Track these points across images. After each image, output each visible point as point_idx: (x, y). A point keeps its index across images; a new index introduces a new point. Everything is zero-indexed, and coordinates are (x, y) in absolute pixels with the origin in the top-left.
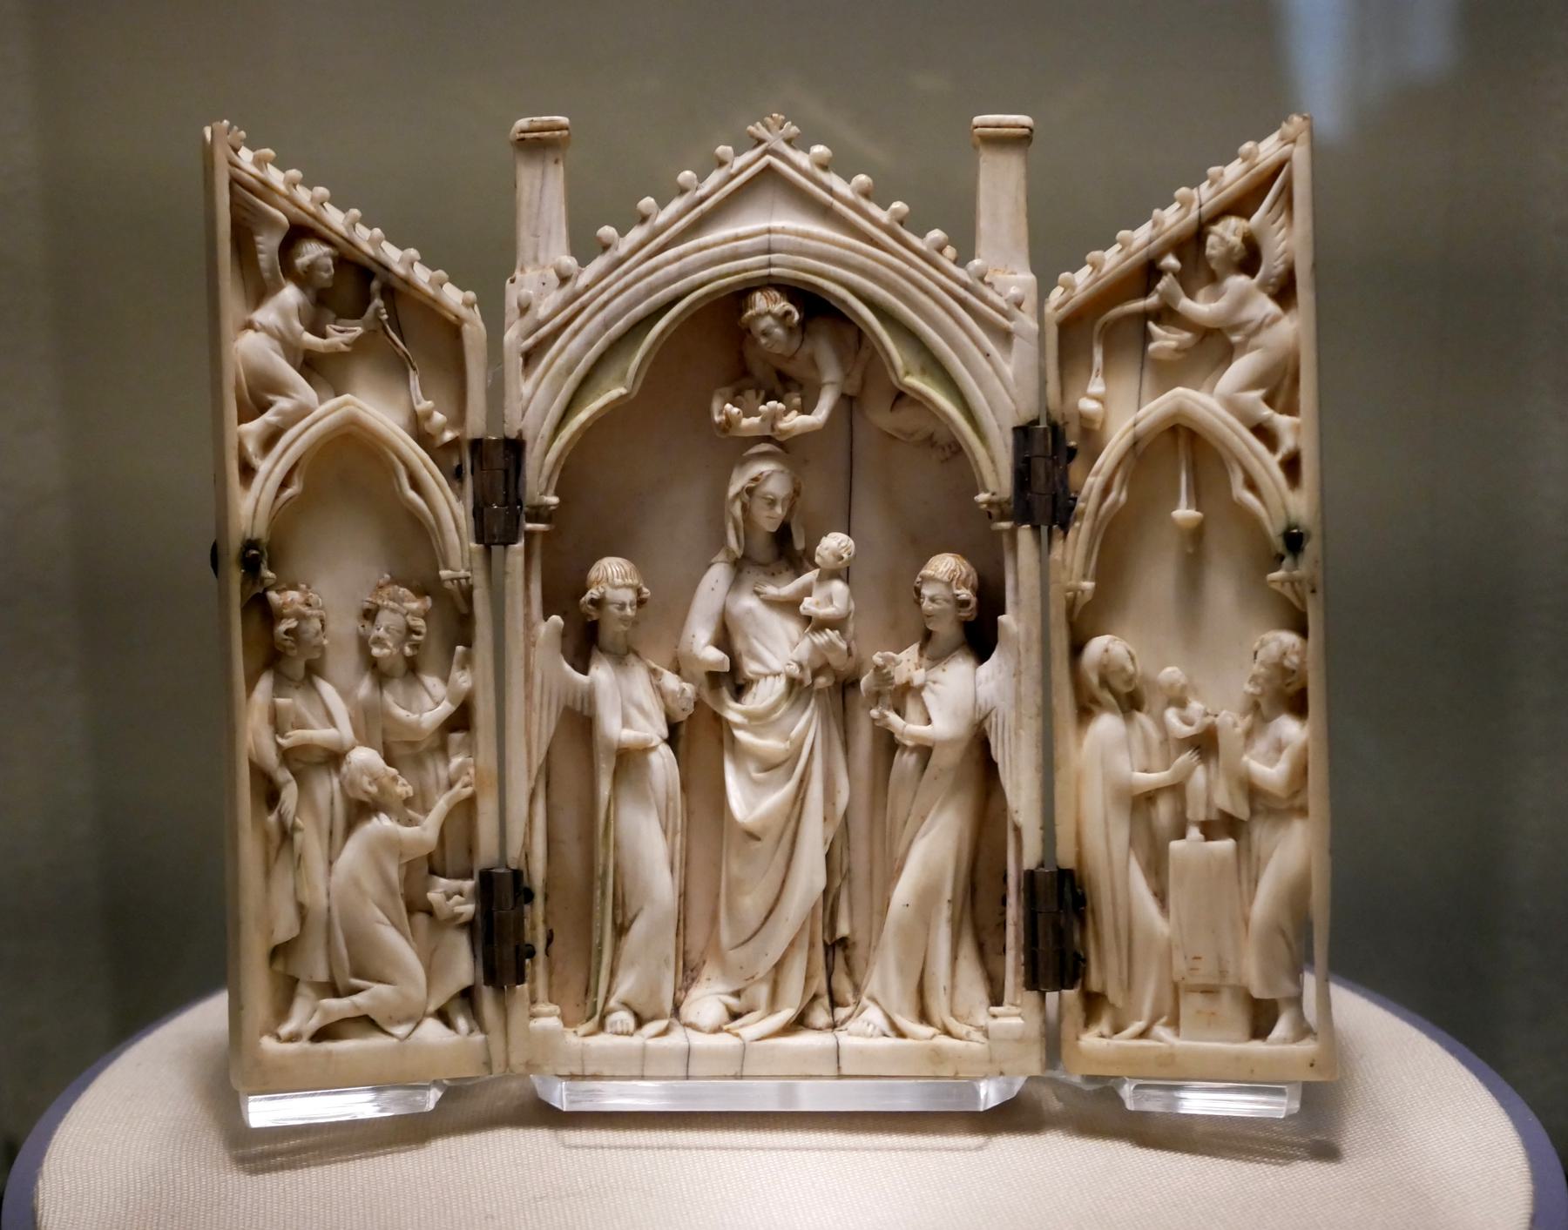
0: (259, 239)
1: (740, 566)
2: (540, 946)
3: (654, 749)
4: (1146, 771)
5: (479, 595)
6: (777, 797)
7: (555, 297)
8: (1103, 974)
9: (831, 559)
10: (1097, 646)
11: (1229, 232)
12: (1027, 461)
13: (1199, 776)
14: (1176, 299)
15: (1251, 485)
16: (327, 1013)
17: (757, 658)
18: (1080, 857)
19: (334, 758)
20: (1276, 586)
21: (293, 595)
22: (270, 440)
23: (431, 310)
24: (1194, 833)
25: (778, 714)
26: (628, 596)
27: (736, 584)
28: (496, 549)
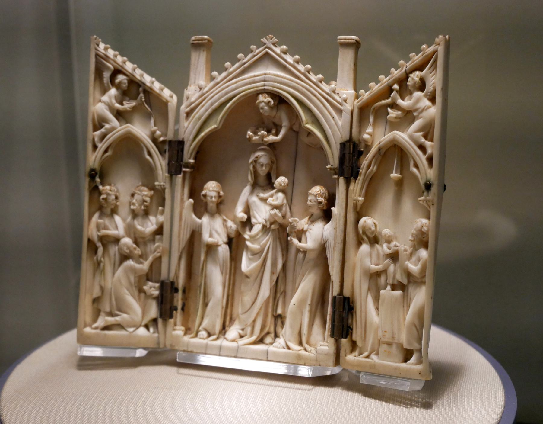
0: (104, 73)
1: (255, 186)
2: (179, 307)
3: (220, 245)
4: (377, 265)
5: (167, 191)
6: (255, 264)
7: (197, 95)
8: (357, 335)
9: (278, 185)
10: (363, 220)
11: (415, 77)
12: (344, 155)
13: (392, 268)
14: (396, 100)
15: (416, 166)
16: (106, 321)
17: (255, 218)
18: (353, 293)
19: (117, 240)
20: (421, 202)
21: (108, 187)
22: (103, 137)
23: (158, 97)
24: (389, 288)
25: (258, 237)
26: (214, 194)
27: (252, 192)
28: (174, 176)
